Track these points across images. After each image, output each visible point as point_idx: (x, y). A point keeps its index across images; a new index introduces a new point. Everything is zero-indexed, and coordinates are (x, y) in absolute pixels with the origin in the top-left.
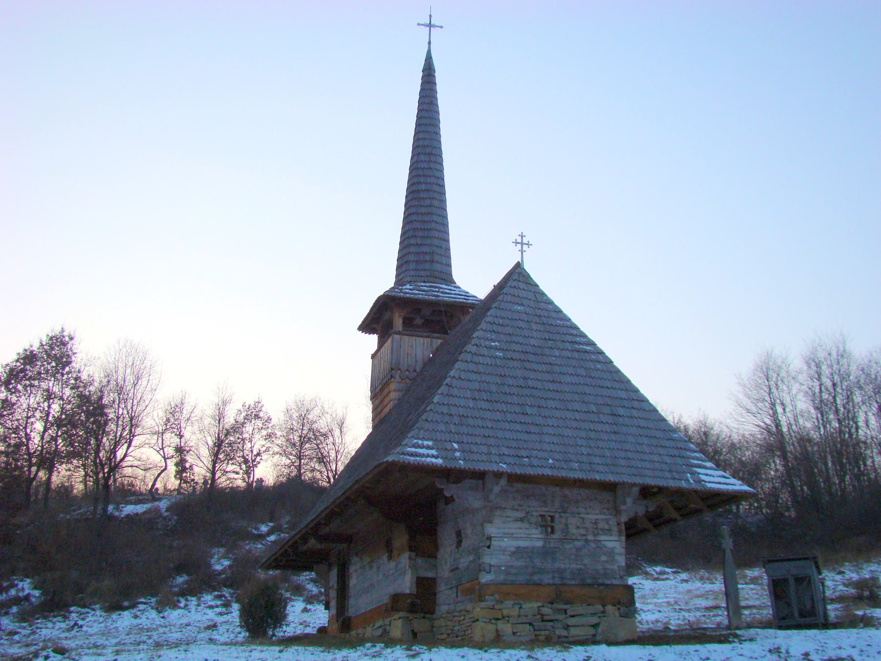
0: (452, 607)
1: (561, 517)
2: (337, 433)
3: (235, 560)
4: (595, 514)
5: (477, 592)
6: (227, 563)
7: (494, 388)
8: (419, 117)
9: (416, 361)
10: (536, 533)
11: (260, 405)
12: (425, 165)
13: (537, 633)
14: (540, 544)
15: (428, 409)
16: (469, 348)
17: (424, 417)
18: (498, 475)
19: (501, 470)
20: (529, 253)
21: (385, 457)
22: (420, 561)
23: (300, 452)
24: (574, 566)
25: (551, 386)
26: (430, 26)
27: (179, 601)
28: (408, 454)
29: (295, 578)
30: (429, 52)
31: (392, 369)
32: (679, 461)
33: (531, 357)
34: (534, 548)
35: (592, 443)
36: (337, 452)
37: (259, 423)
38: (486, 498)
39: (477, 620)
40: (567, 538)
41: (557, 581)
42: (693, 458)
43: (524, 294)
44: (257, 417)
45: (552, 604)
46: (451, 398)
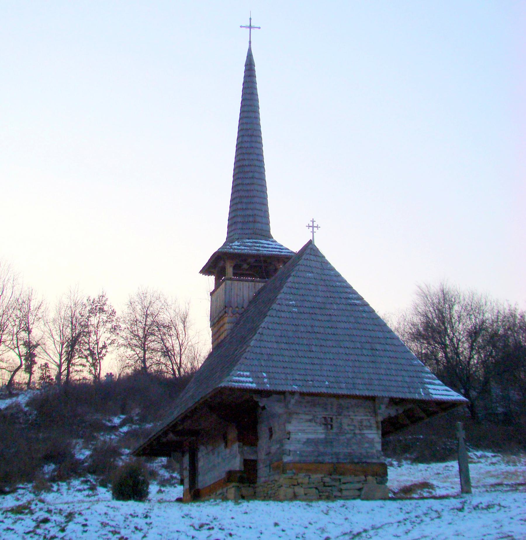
0: (267, 479)
1: (337, 418)
2: (180, 327)
3: (95, 450)
4: (361, 416)
5: (281, 468)
6: (88, 453)
7: (291, 334)
8: (243, 106)
9: (244, 300)
11: (104, 299)
12: (248, 145)
13: (321, 494)
14: (322, 436)
15: (247, 350)
16: (275, 306)
17: (244, 356)
18: (293, 393)
19: (293, 390)
21: (219, 383)
23: (144, 344)
24: (346, 450)
25: (329, 331)
26: (250, 27)
27: (52, 486)
28: (234, 382)
29: (149, 465)
30: (250, 50)
31: (226, 307)
32: (416, 380)
33: (317, 311)
34: (318, 439)
35: (356, 370)
36: (181, 345)
37: (104, 317)
38: (286, 406)
39: (282, 486)
40: (341, 431)
41: (335, 460)
42: (427, 378)
43: (313, 264)
44: (102, 310)
45: (331, 475)
46: (262, 342)
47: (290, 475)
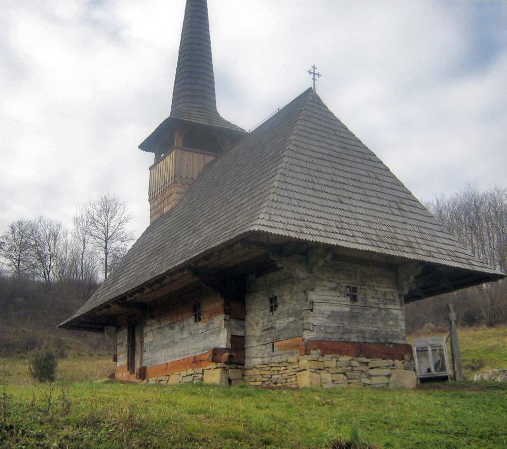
1: (361, 289)
10: (347, 301)
13: (350, 381)
14: (347, 309)
20: (319, 81)
22: (233, 322)
24: (371, 328)
34: (343, 312)
47: (315, 356)
